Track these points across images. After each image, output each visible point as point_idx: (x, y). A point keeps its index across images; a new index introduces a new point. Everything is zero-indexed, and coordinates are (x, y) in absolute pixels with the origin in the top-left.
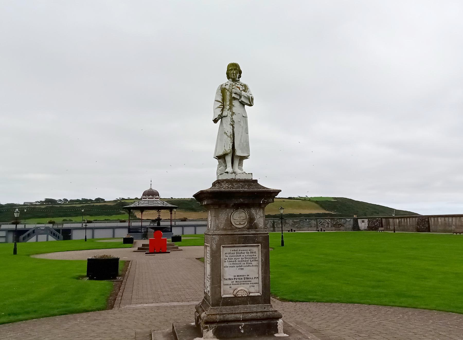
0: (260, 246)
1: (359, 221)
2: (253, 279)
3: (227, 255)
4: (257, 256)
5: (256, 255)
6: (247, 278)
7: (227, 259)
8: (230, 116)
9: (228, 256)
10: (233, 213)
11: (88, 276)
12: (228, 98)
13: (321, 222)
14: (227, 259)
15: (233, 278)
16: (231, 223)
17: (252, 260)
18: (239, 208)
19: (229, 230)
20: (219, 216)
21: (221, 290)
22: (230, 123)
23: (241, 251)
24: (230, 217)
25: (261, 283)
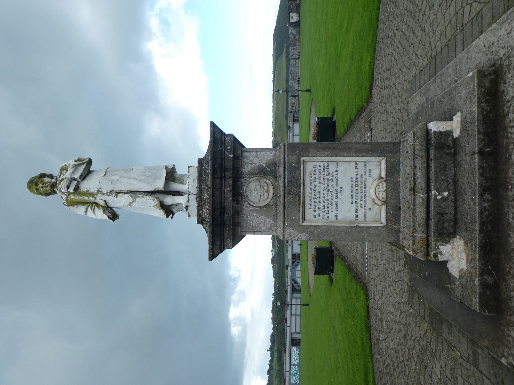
0: (304, 158)
1: (291, 21)
2: (358, 172)
3: (317, 215)
4: (321, 164)
5: (320, 166)
6: (357, 181)
7: (324, 215)
8: (104, 196)
9: (320, 212)
10: (250, 203)
11: (329, 274)
12: (77, 198)
13: (292, 55)
14: (324, 215)
15: (354, 205)
16: (266, 206)
17: (326, 173)
18: (241, 191)
19: (276, 210)
20: (254, 226)
21: (373, 226)
22: (115, 196)
23: (311, 190)
24: (256, 207)
25: (366, 159)
